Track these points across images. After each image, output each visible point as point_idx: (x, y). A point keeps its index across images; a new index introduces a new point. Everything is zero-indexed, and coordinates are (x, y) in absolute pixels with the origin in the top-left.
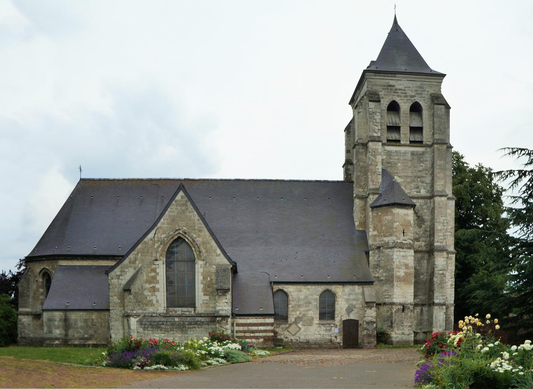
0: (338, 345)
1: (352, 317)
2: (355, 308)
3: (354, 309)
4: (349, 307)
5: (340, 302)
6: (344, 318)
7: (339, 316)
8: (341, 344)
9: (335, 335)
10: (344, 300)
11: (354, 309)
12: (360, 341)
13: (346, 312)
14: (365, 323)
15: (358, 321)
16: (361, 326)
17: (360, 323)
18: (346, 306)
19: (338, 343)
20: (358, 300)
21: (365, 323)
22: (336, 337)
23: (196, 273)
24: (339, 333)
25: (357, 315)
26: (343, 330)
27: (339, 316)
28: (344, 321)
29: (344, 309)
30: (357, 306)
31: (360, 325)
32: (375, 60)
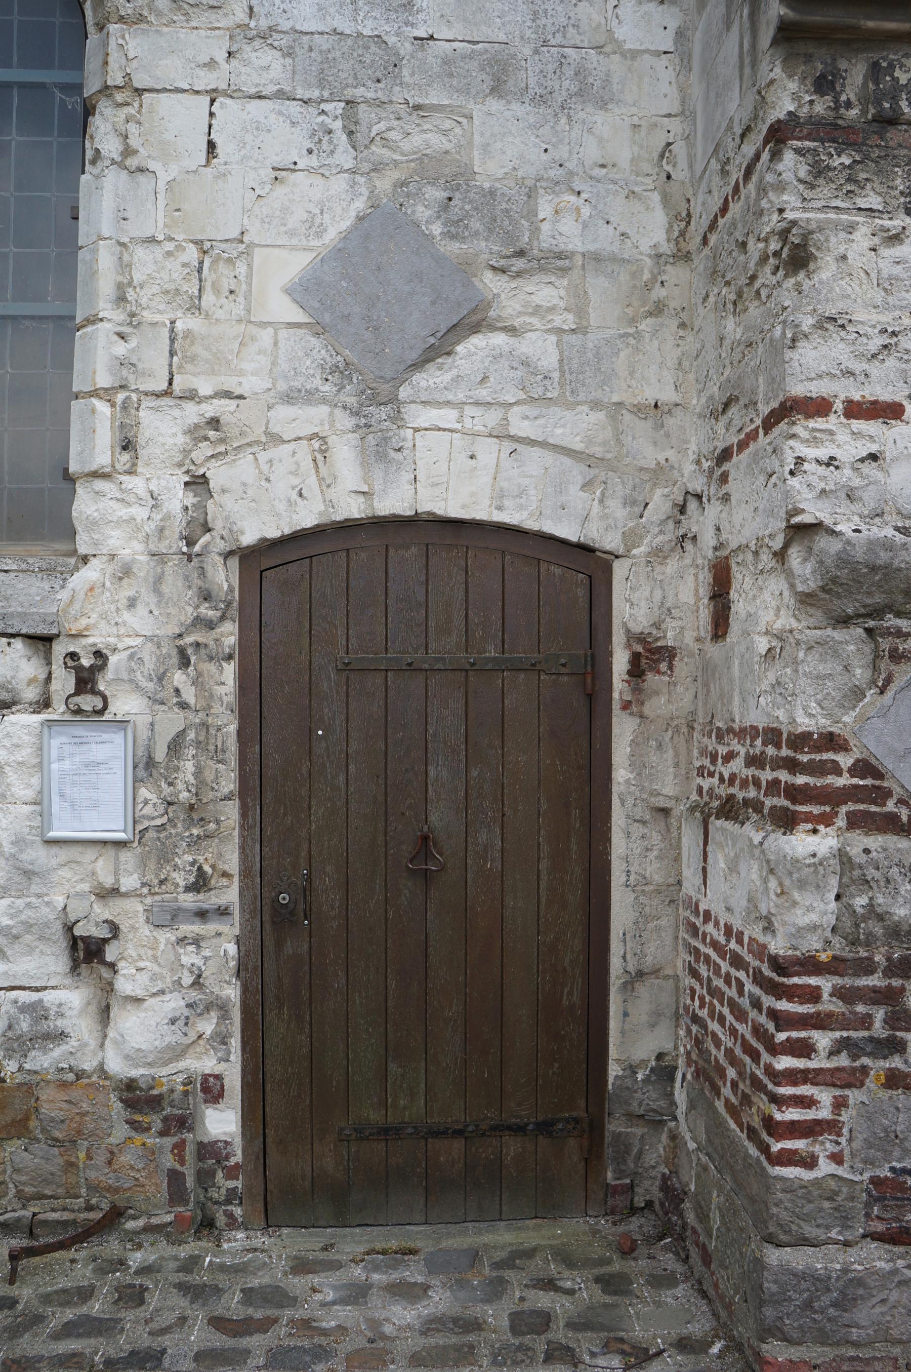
0: (133, 1158)
1: (460, 464)
2: (524, 258)
3: (508, 296)
4: (378, 227)
5: (178, 121)
6: (269, 500)
7: (163, 429)
8: (222, 1123)
9: (66, 889)
10: (265, 66)
11: (508, 296)
12: (635, 1038)
13: (307, 355)
14: (765, 605)
15: (589, 566)
16: (671, 696)
17: (632, 605)
18: (331, 203)
19: (138, 1098)
20: (591, 93)
21: (765, 605)
22: (87, 953)
23: (79, 265)
24: (146, 840)
25: (576, 426)
26: (259, 787)
27: (163, 429)
28: (261, 561)
29: (278, 270)
30: (562, 225)
31: (650, 657)
32: (73, 402)
